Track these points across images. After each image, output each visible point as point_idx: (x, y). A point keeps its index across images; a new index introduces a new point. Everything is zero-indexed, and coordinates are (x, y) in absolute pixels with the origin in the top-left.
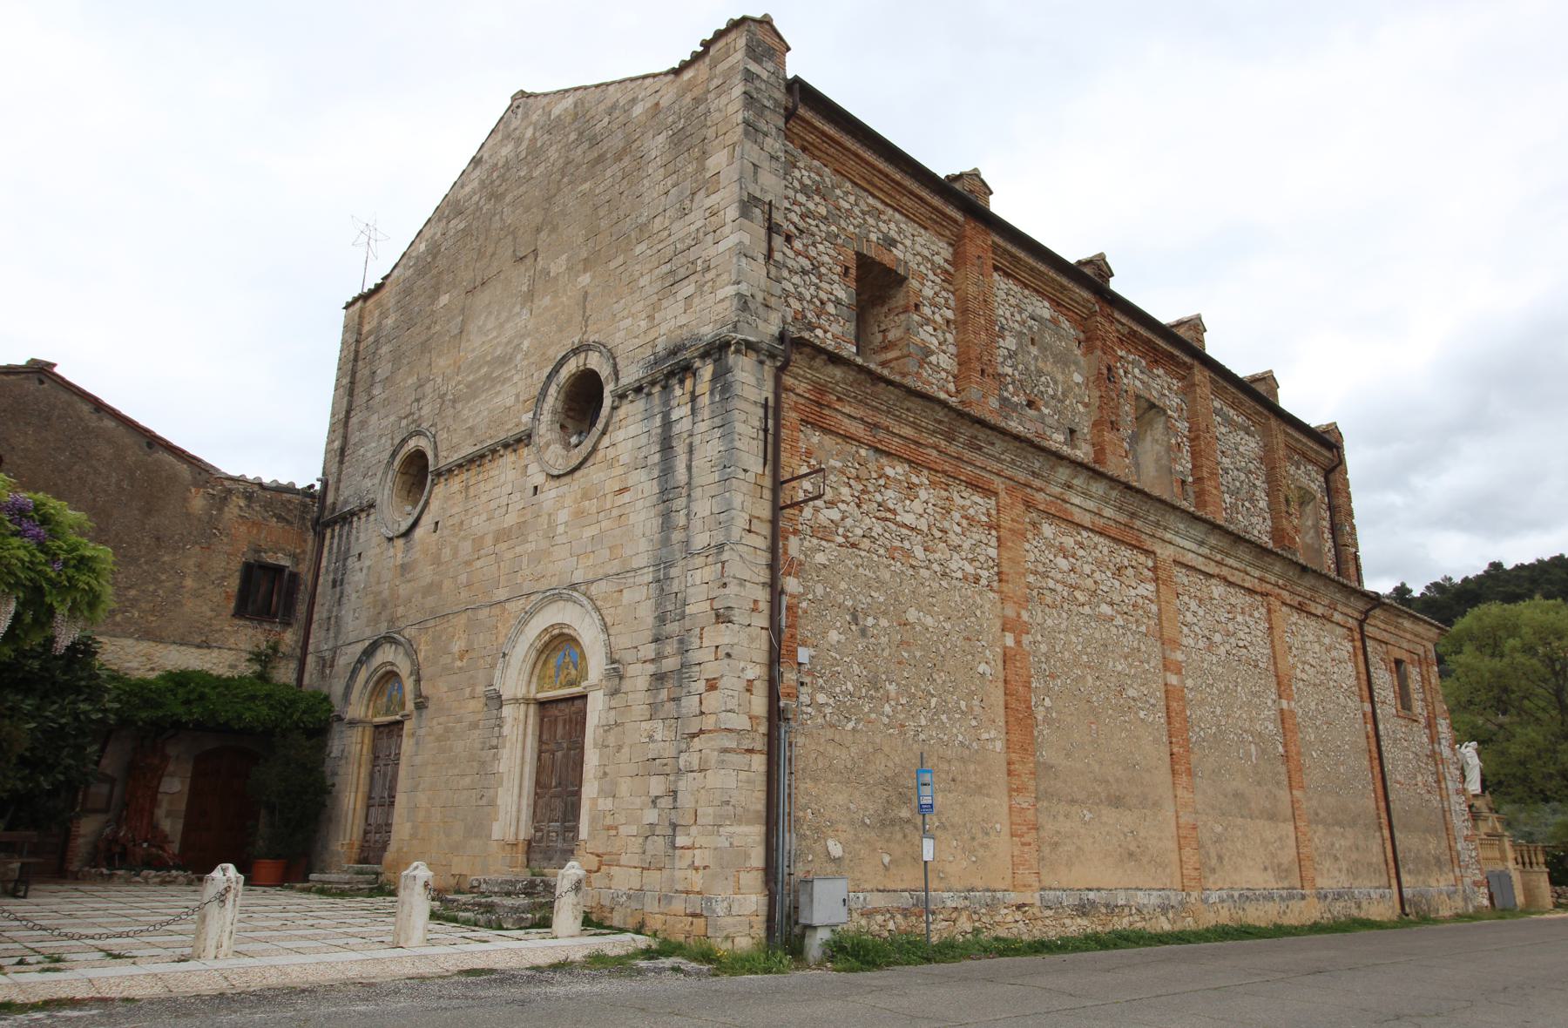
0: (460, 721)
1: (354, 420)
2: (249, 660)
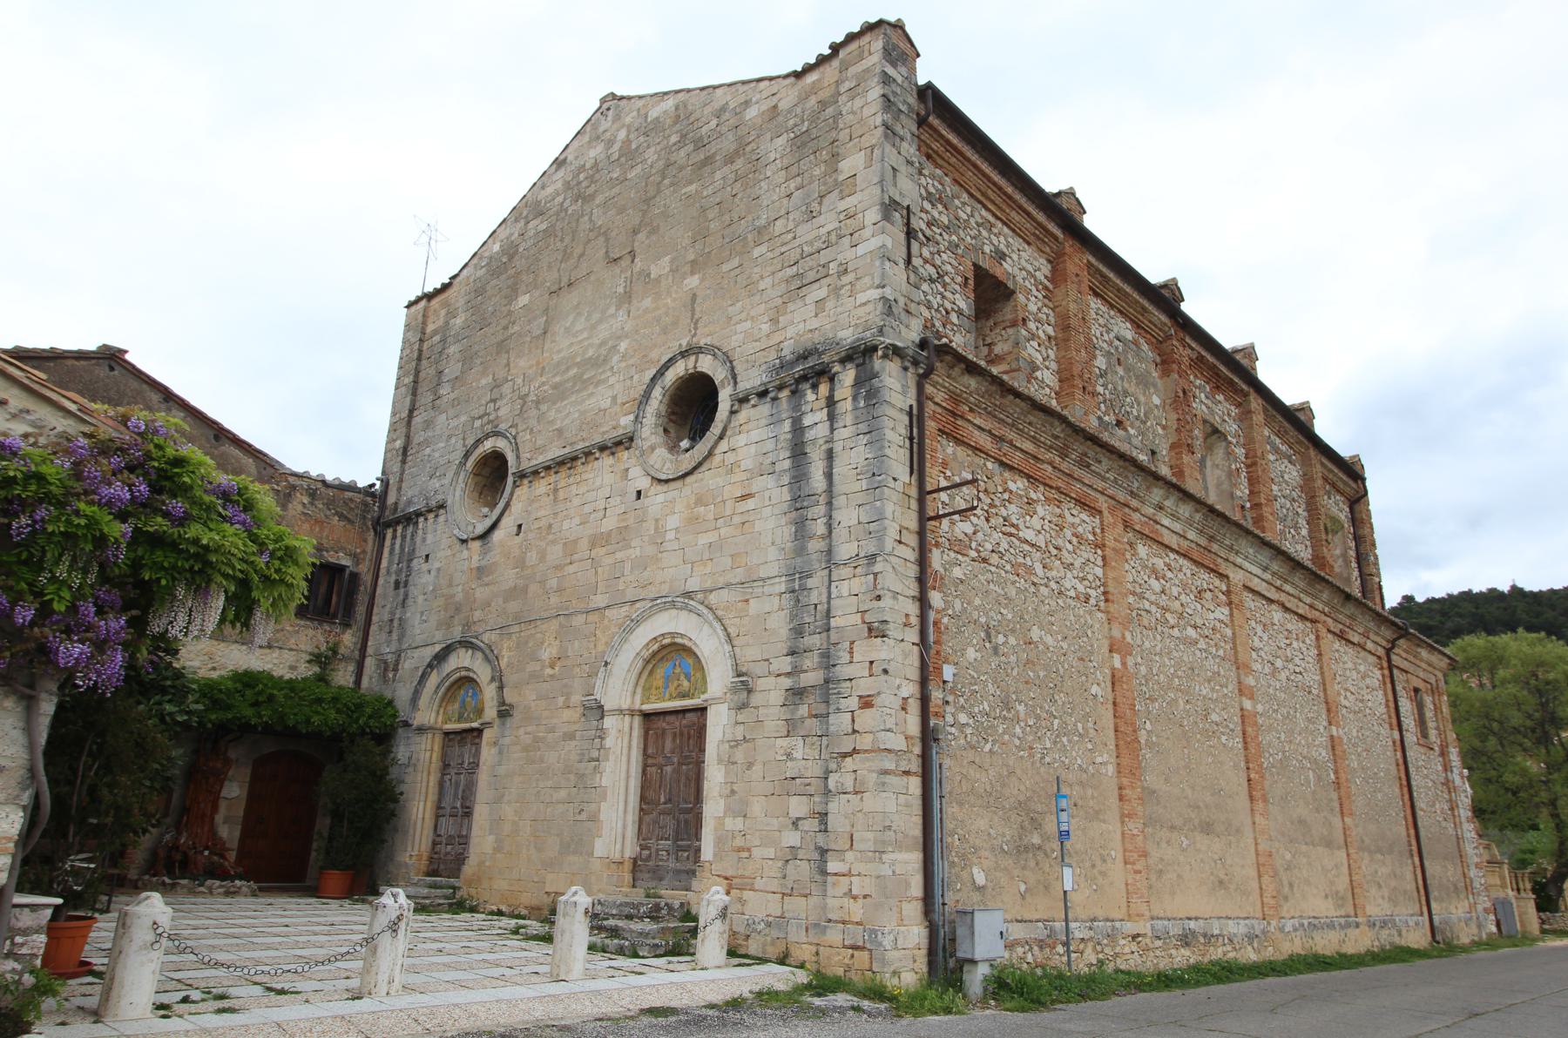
0: (552, 730)
2: (309, 662)
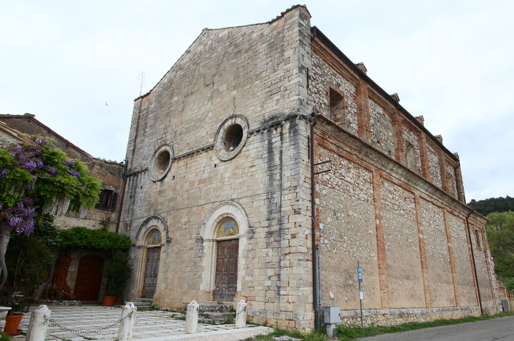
0: (185, 247)
1: (138, 140)
2: (100, 224)
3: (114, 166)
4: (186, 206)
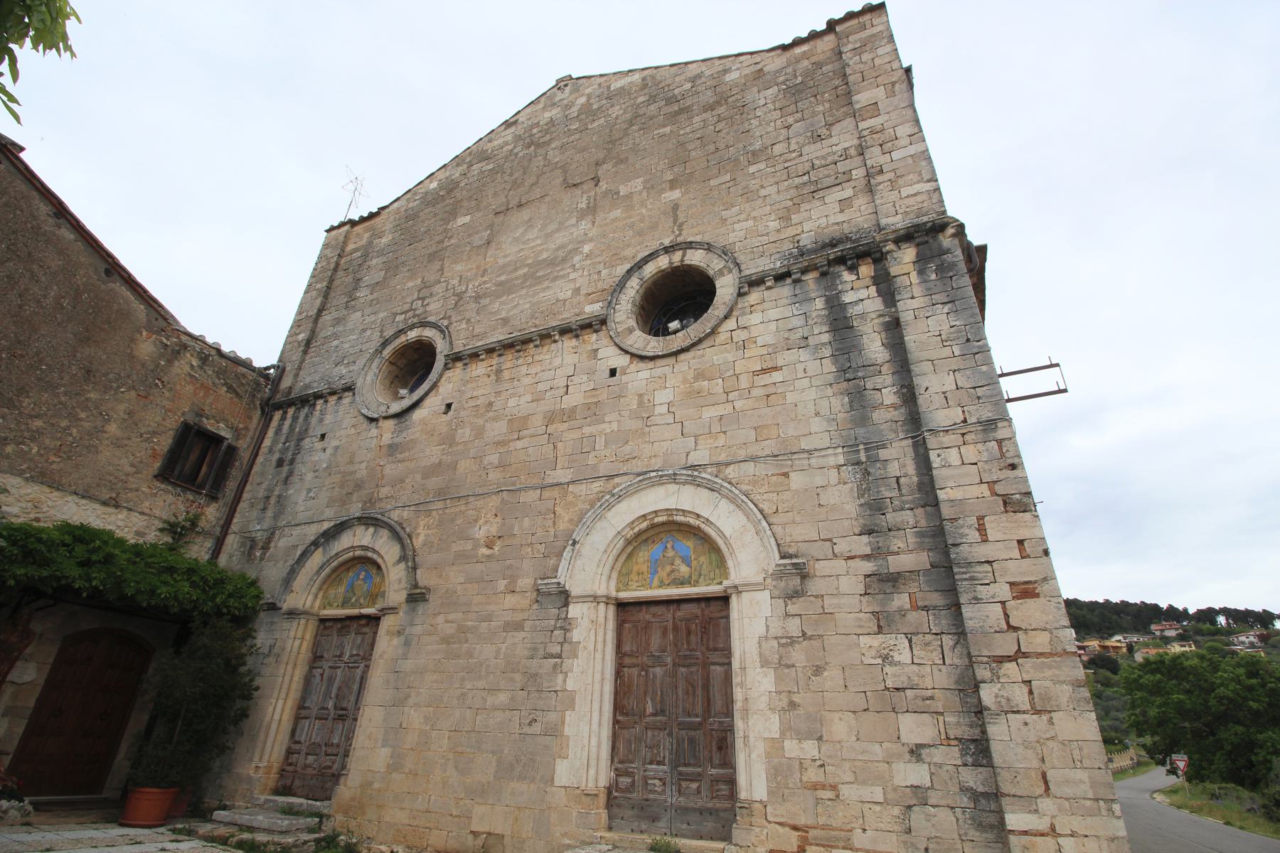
0: (488, 618)
1: (327, 318)
2: (161, 530)
3: (244, 370)
4: (493, 488)
